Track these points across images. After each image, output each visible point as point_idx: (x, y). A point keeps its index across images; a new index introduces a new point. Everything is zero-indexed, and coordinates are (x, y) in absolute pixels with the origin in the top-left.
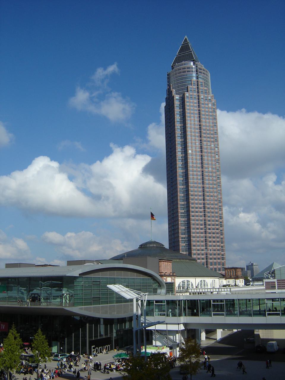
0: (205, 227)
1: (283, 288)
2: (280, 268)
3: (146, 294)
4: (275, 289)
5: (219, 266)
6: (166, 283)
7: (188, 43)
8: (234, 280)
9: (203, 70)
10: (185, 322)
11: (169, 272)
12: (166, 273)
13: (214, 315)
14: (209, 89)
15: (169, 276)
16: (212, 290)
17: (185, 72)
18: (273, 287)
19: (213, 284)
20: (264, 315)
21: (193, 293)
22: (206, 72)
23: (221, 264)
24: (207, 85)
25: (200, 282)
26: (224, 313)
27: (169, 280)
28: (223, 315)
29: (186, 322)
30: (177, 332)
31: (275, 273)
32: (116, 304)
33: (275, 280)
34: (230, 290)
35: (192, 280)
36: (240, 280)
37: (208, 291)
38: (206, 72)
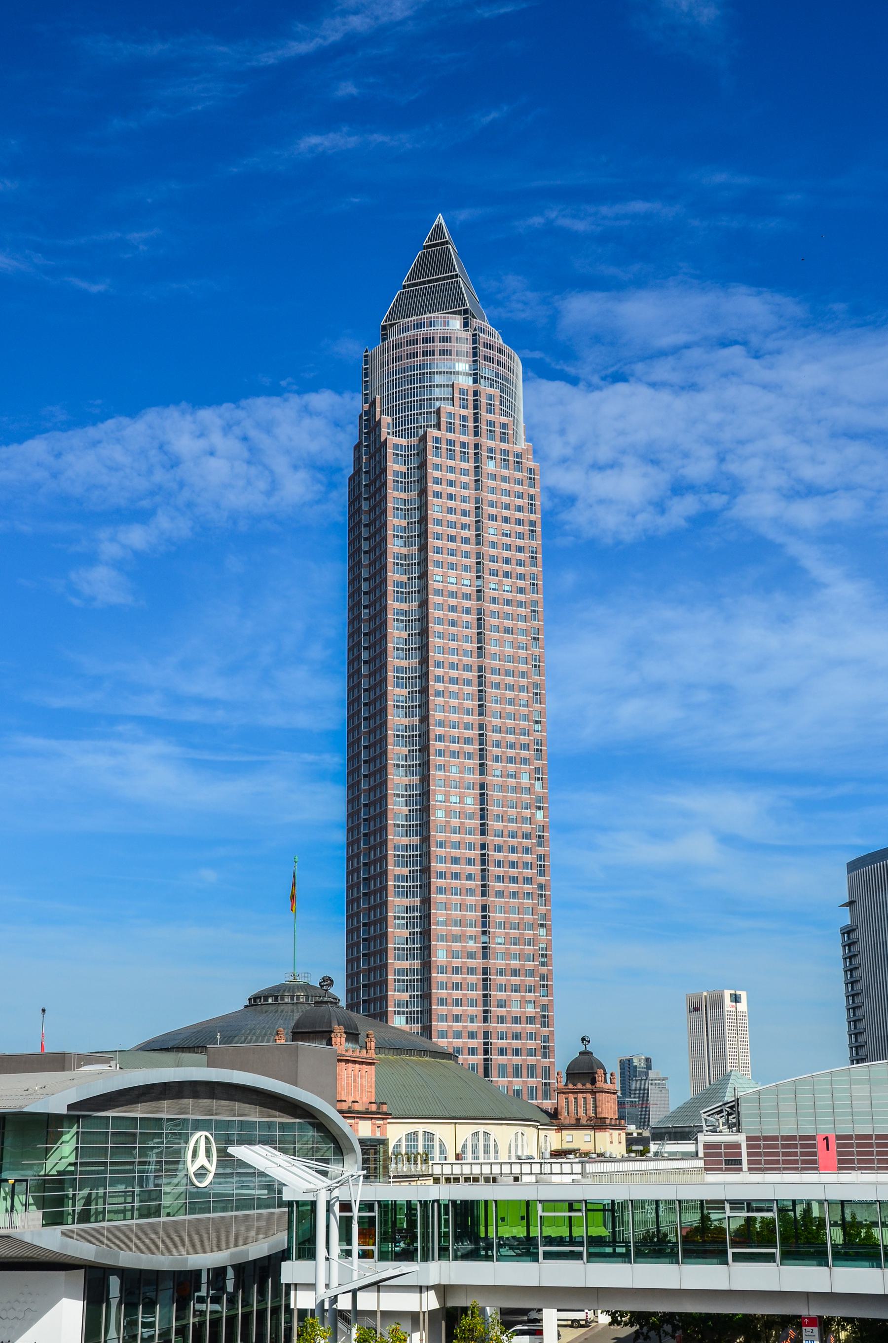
0: (484, 933)
1: (767, 1169)
2: (759, 1091)
3: (360, 1176)
4: (741, 1169)
5: (532, 1081)
6: (362, 1142)
7: (446, 243)
8: (588, 1132)
9: (500, 351)
10: (442, 1283)
11: (365, 1099)
12: (354, 1102)
13: (738, 1257)
14: (515, 422)
15: (366, 1115)
16: (516, 1169)
17: (415, 355)
18: (733, 1164)
19: (516, 1146)
20: (720, 1256)
21: (448, 1180)
22: (509, 357)
23: (539, 1071)
24: (512, 407)
25: (470, 1141)
26: (773, 1251)
27: (365, 1129)
28: (770, 1258)
29: (448, 1283)
30: (414, 1317)
31: (738, 1112)
32: (188, 1217)
33: (741, 1138)
34: (583, 1169)
35: (443, 1132)
36: (611, 1134)
37: (501, 1174)
38: (509, 357)
